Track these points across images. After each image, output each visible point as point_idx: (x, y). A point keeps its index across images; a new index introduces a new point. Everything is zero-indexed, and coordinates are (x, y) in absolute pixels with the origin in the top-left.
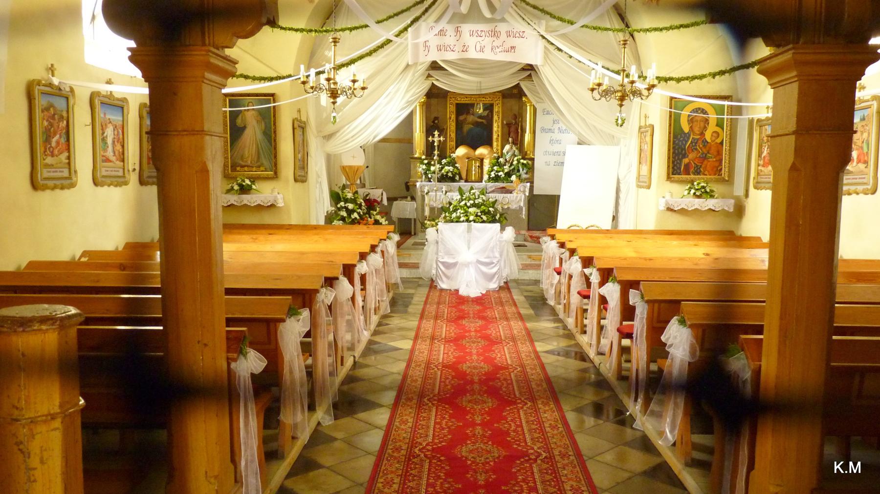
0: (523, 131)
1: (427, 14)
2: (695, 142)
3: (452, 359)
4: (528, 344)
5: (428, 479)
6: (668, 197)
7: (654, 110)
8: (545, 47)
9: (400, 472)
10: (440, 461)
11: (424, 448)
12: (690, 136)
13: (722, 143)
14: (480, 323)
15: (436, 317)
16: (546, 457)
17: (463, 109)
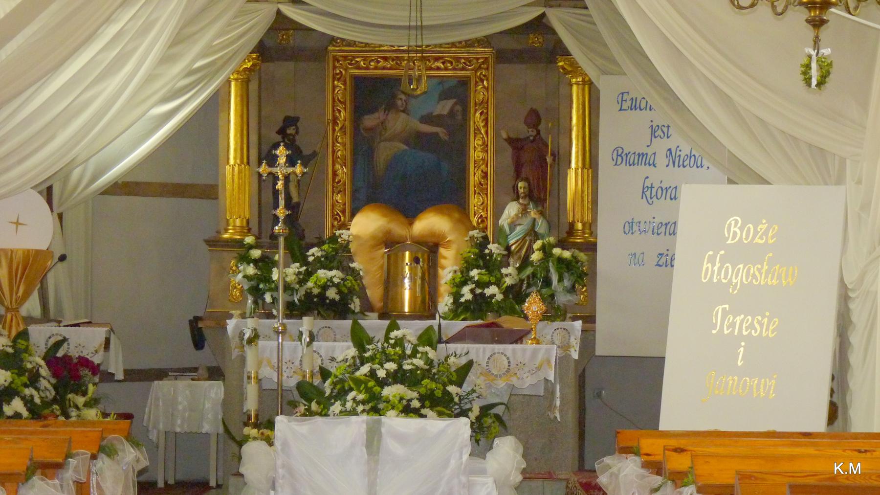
0: (562, 159)
17: (373, 93)
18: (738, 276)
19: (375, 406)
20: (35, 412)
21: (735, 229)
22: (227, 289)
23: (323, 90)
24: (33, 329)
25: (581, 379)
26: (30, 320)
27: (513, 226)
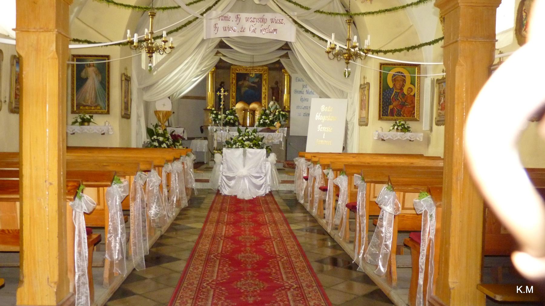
0: (283, 92)
1: (216, 6)
2: (397, 94)
3: (231, 233)
4: (285, 225)
5: (213, 300)
6: (380, 131)
7: (369, 71)
8: (297, 30)
9: (193, 297)
10: (222, 290)
11: (210, 283)
12: (393, 90)
13: (414, 95)
14: (251, 214)
15: (221, 210)
16: (297, 287)
17: (241, 77)
18: (323, 118)
19: (243, 146)
20: (169, 147)
21: (323, 108)
22: (208, 120)
23: (230, 76)
24: (168, 128)
25: (286, 140)
26: (166, 126)
27: (272, 107)
